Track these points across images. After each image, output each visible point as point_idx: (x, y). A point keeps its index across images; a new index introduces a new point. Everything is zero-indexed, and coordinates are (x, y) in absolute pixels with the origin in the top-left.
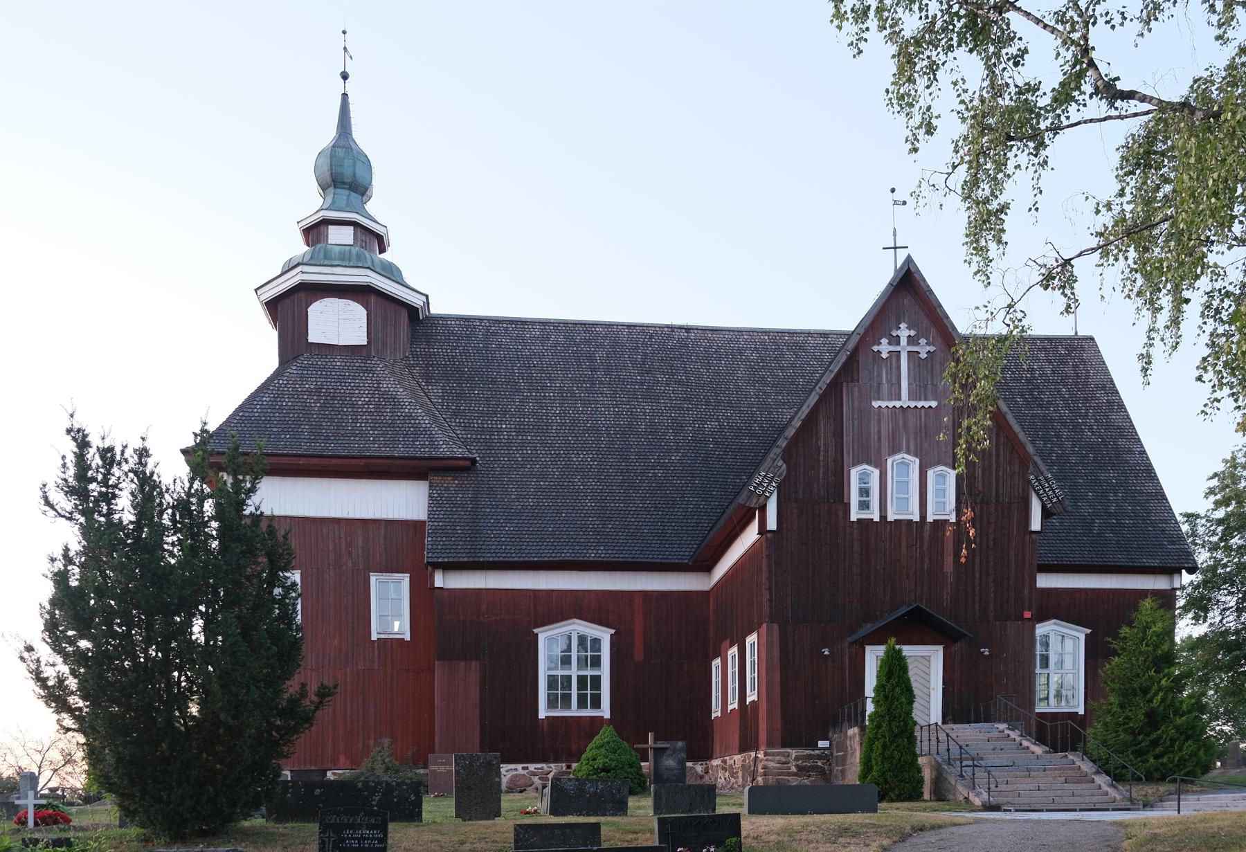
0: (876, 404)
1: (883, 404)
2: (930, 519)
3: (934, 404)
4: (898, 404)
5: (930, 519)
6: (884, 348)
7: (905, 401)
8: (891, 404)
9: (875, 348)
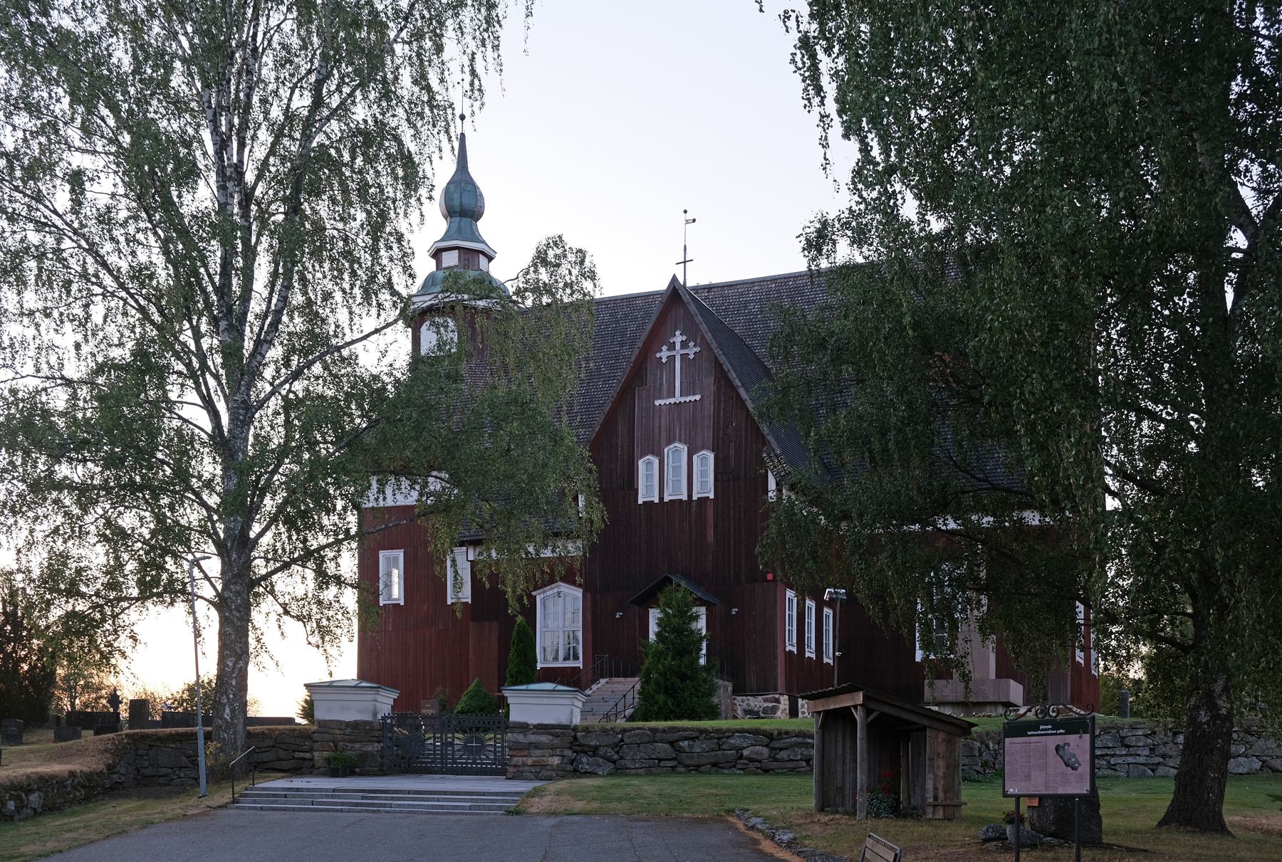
0: (657, 403)
1: (662, 402)
2: (695, 498)
3: (698, 397)
4: (672, 401)
5: (695, 498)
6: (664, 354)
7: (678, 399)
9: (658, 355)
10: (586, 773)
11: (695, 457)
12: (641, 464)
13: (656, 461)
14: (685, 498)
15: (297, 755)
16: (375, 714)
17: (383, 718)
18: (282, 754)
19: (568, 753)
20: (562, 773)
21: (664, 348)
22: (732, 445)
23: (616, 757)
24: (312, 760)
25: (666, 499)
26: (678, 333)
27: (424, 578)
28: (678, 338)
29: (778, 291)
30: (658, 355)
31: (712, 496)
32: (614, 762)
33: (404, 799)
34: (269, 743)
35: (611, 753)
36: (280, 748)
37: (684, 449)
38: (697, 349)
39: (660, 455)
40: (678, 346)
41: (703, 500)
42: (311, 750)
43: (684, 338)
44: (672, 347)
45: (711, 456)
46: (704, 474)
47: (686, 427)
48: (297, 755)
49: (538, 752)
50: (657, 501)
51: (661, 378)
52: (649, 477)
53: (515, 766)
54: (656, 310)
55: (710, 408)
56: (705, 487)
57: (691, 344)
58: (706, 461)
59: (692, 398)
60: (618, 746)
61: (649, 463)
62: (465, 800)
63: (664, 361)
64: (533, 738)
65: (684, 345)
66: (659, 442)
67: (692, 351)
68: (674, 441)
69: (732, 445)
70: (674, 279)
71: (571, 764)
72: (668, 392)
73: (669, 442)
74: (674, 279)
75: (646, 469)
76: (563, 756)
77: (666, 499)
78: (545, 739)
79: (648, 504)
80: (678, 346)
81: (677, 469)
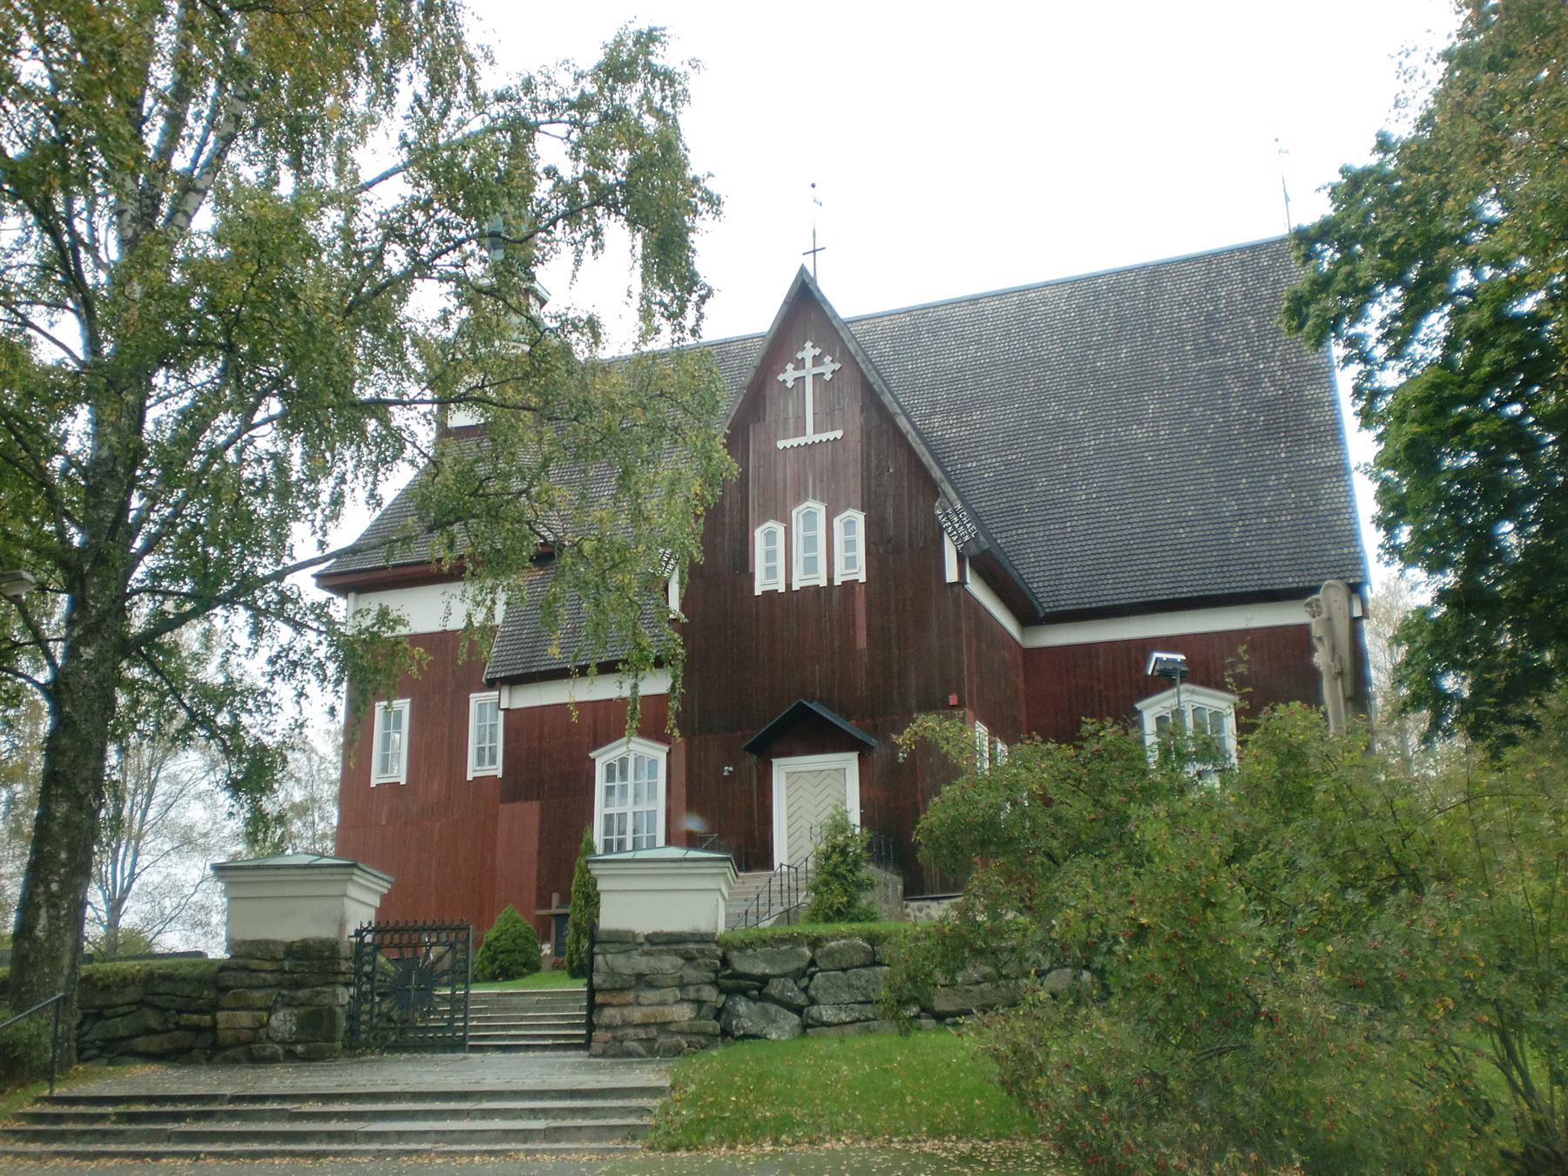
0: (781, 444)
2: (837, 582)
3: (839, 434)
4: (802, 441)
5: (837, 582)
6: (789, 375)
7: (810, 437)
8: (795, 442)
9: (781, 378)
10: (746, 1036)
11: (837, 522)
12: (759, 535)
13: (779, 529)
14: (823, 583)
15: (186, 1018)
16: (342, 925)
17: (358, 933)
18: (153, 1020)
19: (709, 994)
20: (702, 1040)
21: (790, 367)
22: (890, 501)
23: (801, 999)
24: (213, 1028)
25: (795, 587)
26: (808, 344)
27: (439, 738)
28: (809, 352)
29: (915, 326)
30: (781, 378)
31: (862, 578)
32: (798, 1010)
33: (456, 1114)
34: (132, 994)
35: (793, 993)
36: (177, 1011)
37: (820, 509)
38: (837, 366)
39: (786, 520)
40: (809, 363)
41: (849, 586)
42: (214, 1007)
43: (818, 351)
44: (800, 364)
45: (859, 518)
46: (850, 545)
47: (820, 475)
48: (186, 1018)
49: (650, 996)
50: (782, 589)
51: (786, 410)
52: (771, 555)
53: (608, 1027)
54: (755, 358)
55: (855, 446)
56: (852, 566)
57: (828, 359)
58: (853, 525)
59: (831, 435)
60: (803, 974)
61: (770, 536)
62: (534, 1113)
63: (790, 385)
64: (641, 963)
65: (817, 360)
66: (785, 503)
67: (829, 367)
68: (806, 500)
69: (890, 501)
70: (803, 270)
71: (717, 1018)
72: (796, 428)
73: (799, 499)
74: (803, 270)
75: (765, 541)
76: (699, 1003)
77: (795, 587)
78: (669, 963)
79: (770, 595)
80: (809, 363)
81: (810, 543)
